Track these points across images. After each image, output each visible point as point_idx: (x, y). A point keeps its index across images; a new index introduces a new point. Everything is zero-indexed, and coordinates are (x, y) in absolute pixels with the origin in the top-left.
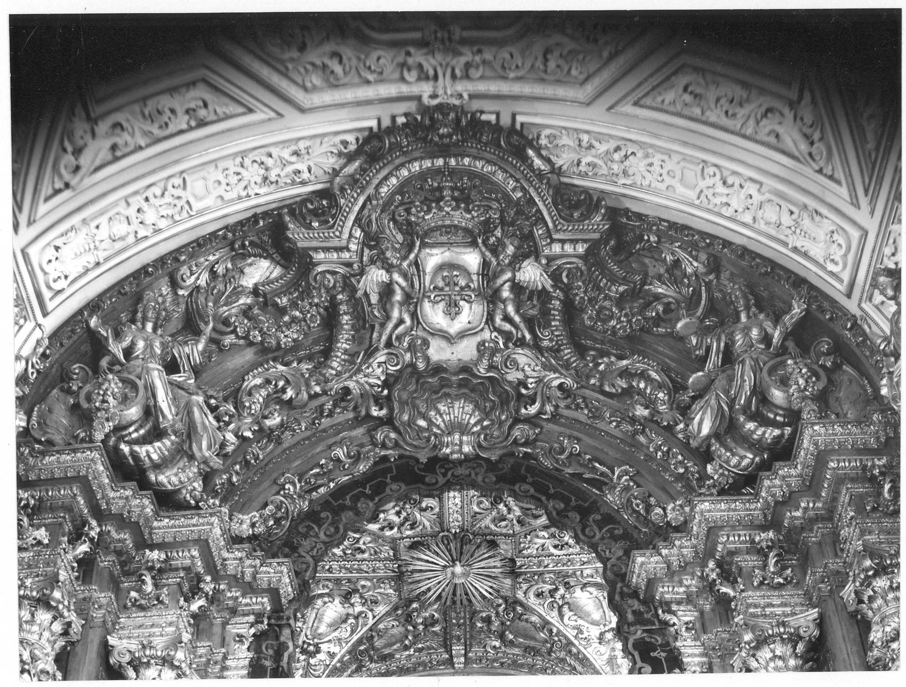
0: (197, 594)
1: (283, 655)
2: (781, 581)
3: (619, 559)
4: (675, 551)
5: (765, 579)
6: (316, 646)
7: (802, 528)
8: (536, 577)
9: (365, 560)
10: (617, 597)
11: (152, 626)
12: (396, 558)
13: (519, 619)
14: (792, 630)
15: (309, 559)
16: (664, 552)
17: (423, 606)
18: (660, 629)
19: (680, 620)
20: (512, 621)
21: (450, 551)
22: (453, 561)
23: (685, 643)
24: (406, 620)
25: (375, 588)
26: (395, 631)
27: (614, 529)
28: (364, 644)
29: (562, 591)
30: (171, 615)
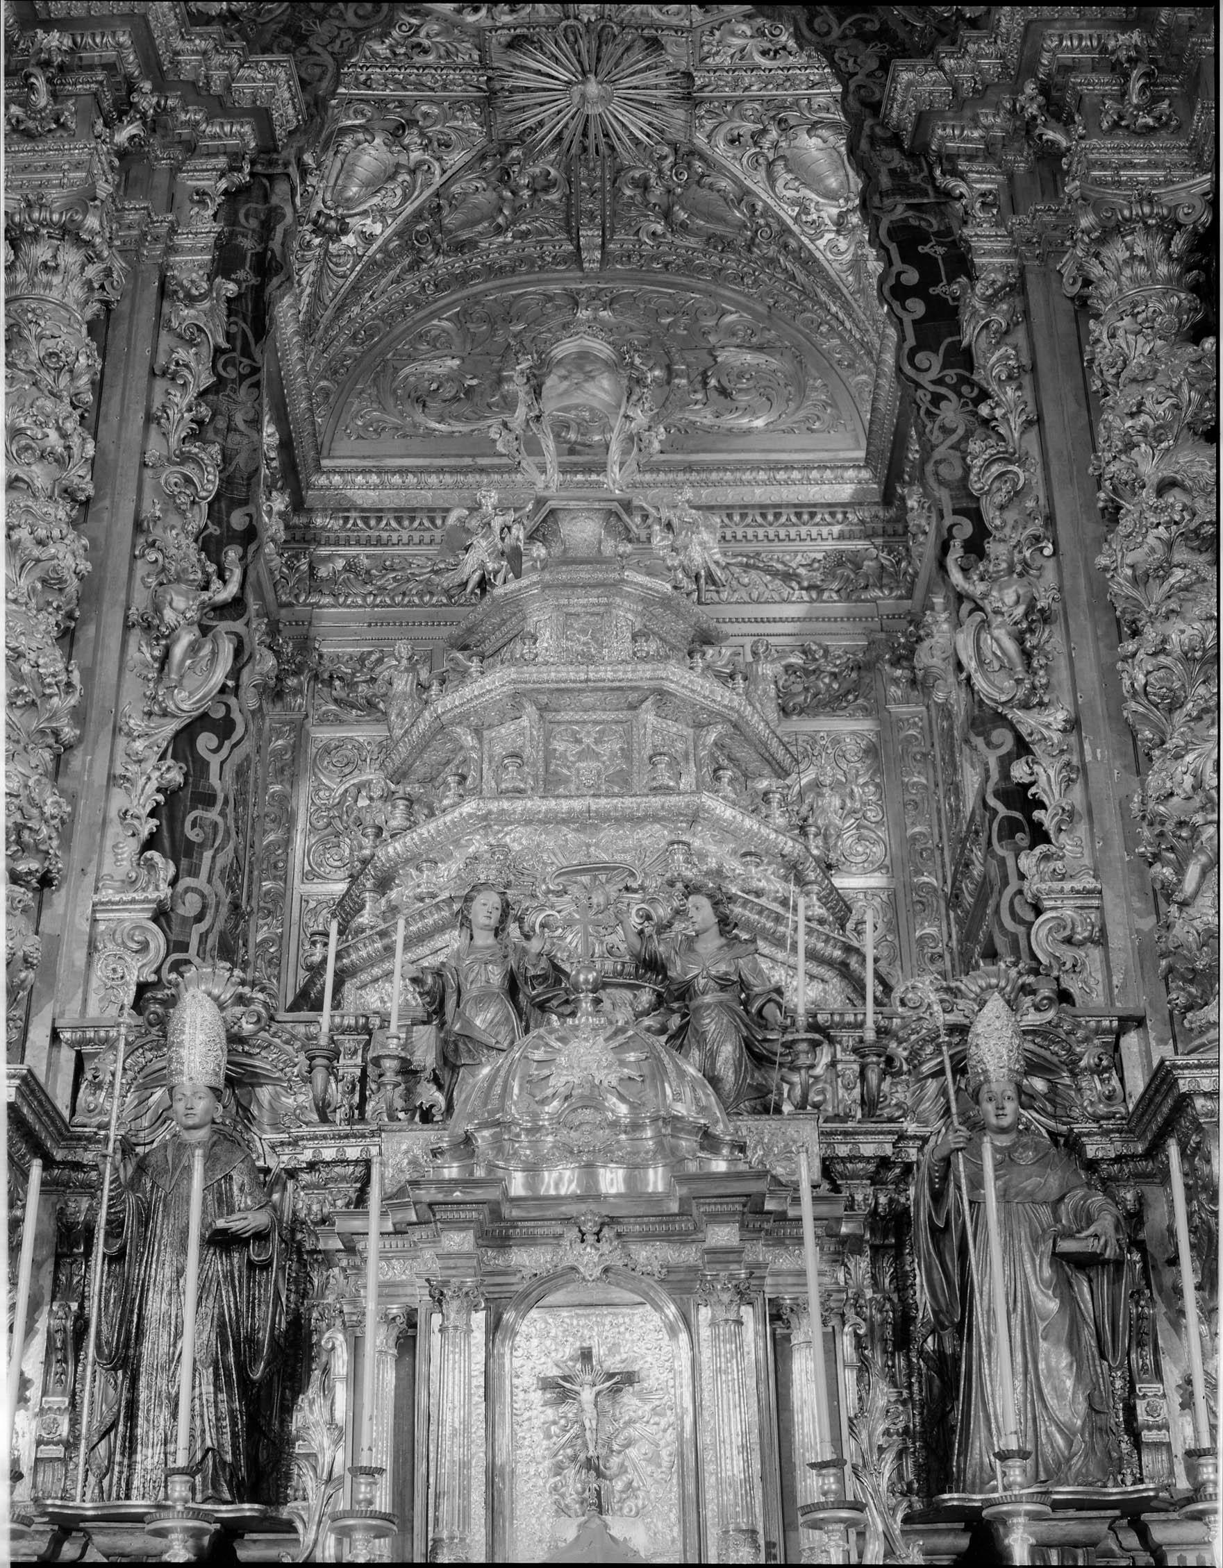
0: (126, 113)
1: (274, 228)
2: (1150, 121)
3: (870, 75)
4: (967, 62)
5: (1121, 118)
6: (341, 220)
7: (1191, 27)
8: (729, 108)
9: (428, 67)
10: (864, 144)
11: (45, 168)
12: (484, 65)
13: (698, 183)
14: (1165, 211)
15: (327, 59)
16: (949, 63)
17: (531, 154)
18: (938, 204)
19: (971, 188)
20: (686, 186)
21: (578, 54)
22: (584, 73)
23: (979, 231)
24: (501, 180)
25: (446, 120)
26: (480, 198)
27: (865, 21)
28: (425, 220)
29: (774, 134)
30: (78, 152)
